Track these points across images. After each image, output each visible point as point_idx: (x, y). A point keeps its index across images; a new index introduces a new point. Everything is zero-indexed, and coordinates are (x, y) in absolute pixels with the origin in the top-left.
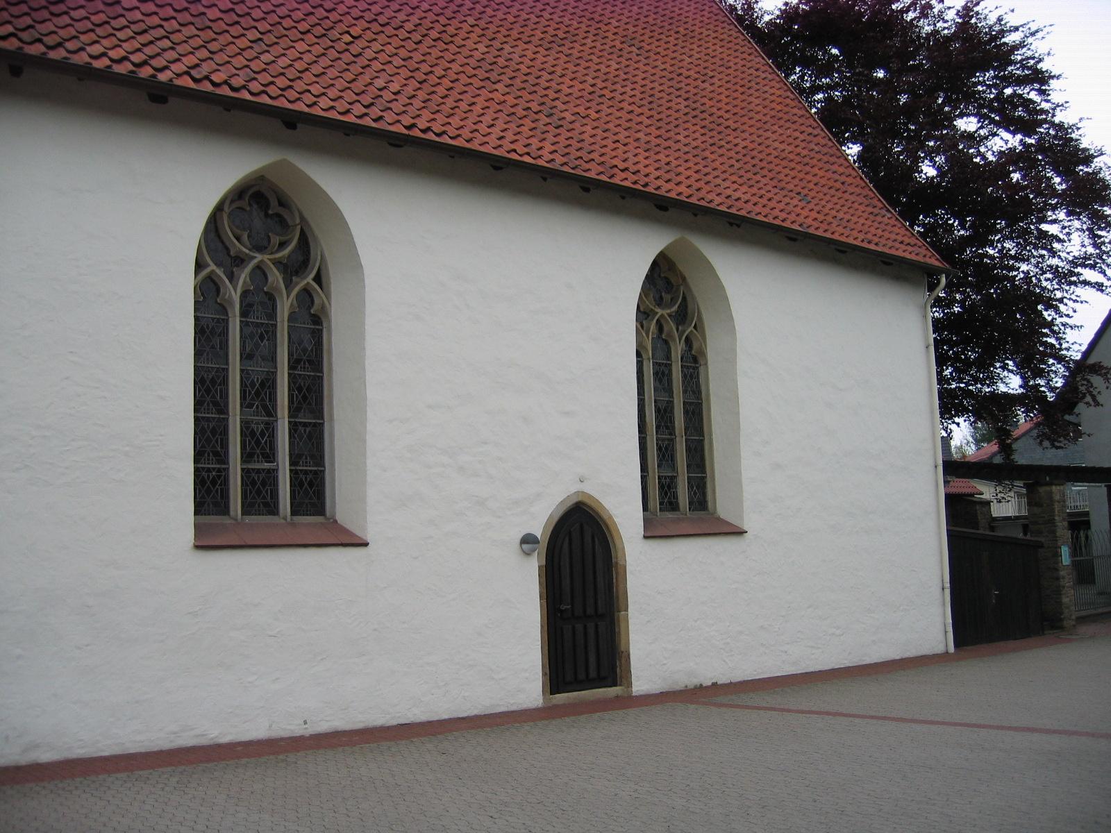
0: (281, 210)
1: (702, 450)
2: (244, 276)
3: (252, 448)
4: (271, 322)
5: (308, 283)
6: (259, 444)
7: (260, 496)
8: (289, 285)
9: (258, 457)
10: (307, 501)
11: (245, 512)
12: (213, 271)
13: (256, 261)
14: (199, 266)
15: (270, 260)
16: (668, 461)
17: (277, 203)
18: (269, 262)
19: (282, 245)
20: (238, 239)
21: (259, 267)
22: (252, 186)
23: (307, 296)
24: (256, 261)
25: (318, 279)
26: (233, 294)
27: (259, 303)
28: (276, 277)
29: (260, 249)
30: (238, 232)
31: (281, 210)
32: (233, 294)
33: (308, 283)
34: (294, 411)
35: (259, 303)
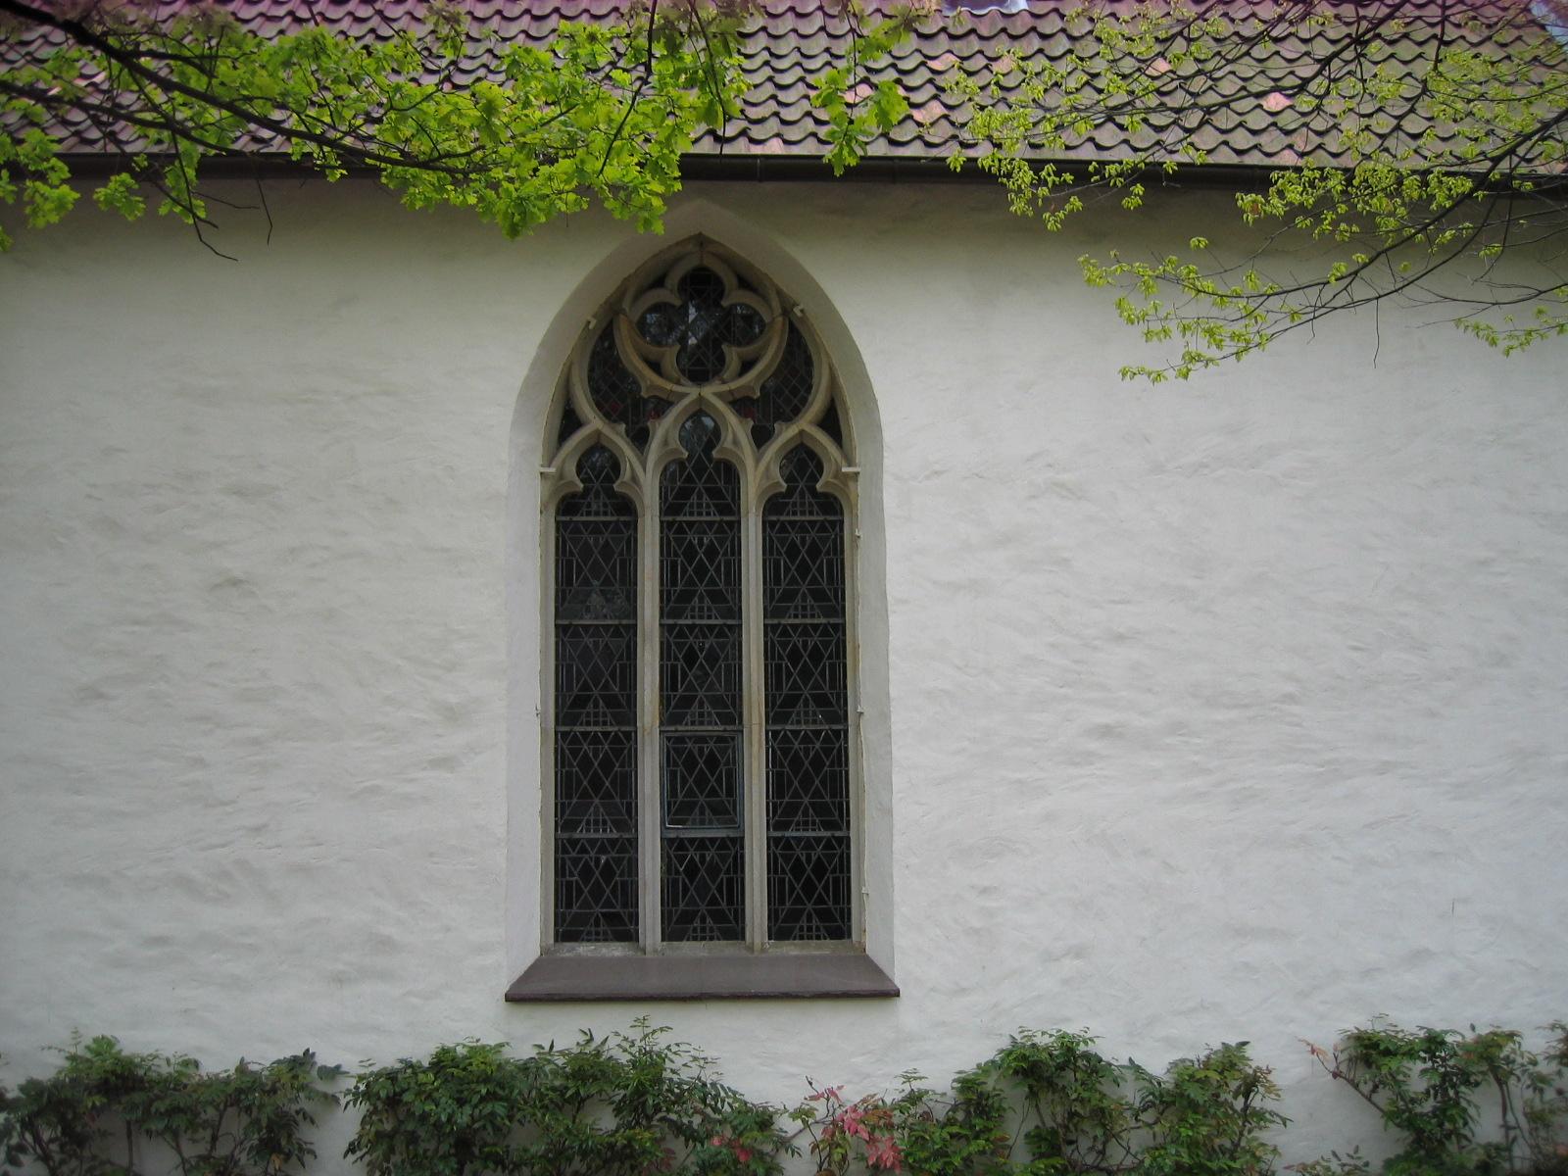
0: (673, 280)
1: (841, 759)
2: (665, 430)
3: (690, 793)
4: (622, 519)
5: (802, 433)
6: (705, 780)
7: (704, 900)
8: (761, 437)
9: (702, 813)
10: (598, 910)
11: (668, 935)
12: (598, 433)
13: (686, 402)
14: (568, 422)
15: (720, 395)
16: (608, 795)
17: (734, 281)
18: (720, 405)
19: (746, 366)
20: (655, 366)
21: (698, 412)
22: (677, 260)
23: (803, 462)
24: (686, 402)
25: (832, 422)
26: (645, 479)
27: (701, 481)
28: (737, 431)
29: (699, 376)
30: (654, 351)
31: (673, 280)
32: (645, 479)
33: (802, 433)
34: (778, 709)
35: (701, 481)
